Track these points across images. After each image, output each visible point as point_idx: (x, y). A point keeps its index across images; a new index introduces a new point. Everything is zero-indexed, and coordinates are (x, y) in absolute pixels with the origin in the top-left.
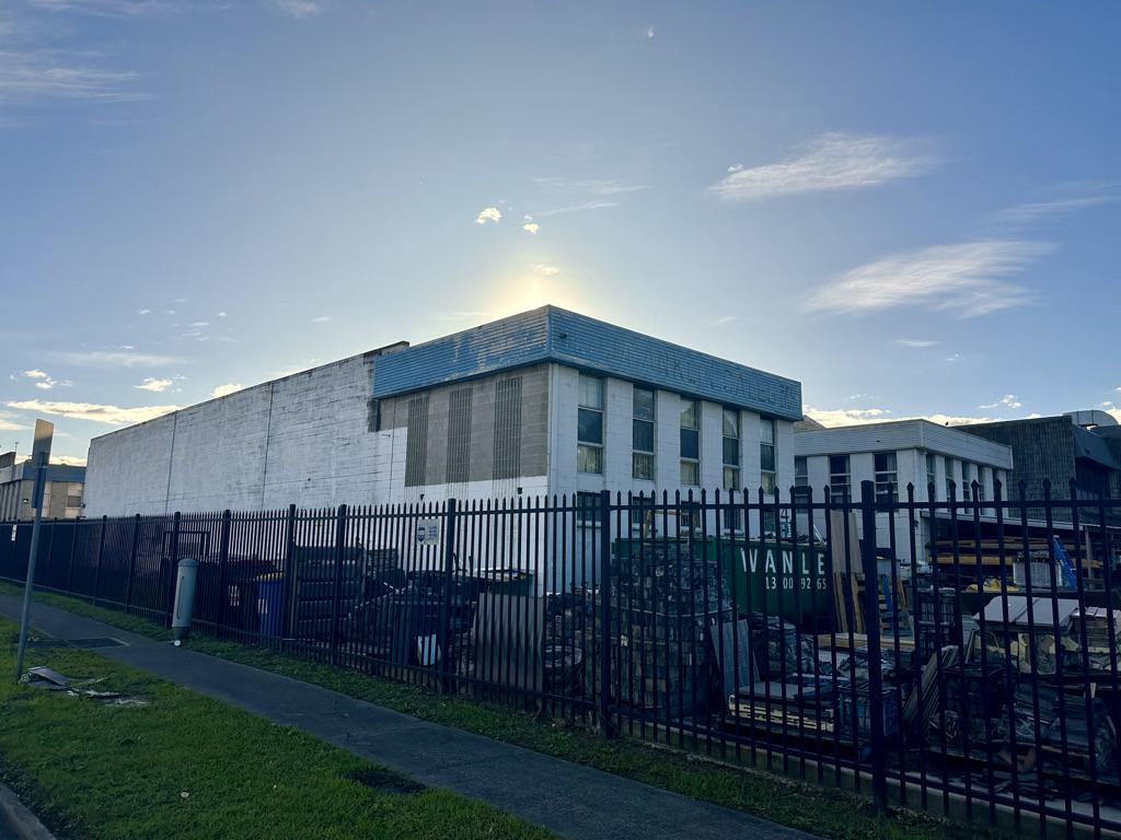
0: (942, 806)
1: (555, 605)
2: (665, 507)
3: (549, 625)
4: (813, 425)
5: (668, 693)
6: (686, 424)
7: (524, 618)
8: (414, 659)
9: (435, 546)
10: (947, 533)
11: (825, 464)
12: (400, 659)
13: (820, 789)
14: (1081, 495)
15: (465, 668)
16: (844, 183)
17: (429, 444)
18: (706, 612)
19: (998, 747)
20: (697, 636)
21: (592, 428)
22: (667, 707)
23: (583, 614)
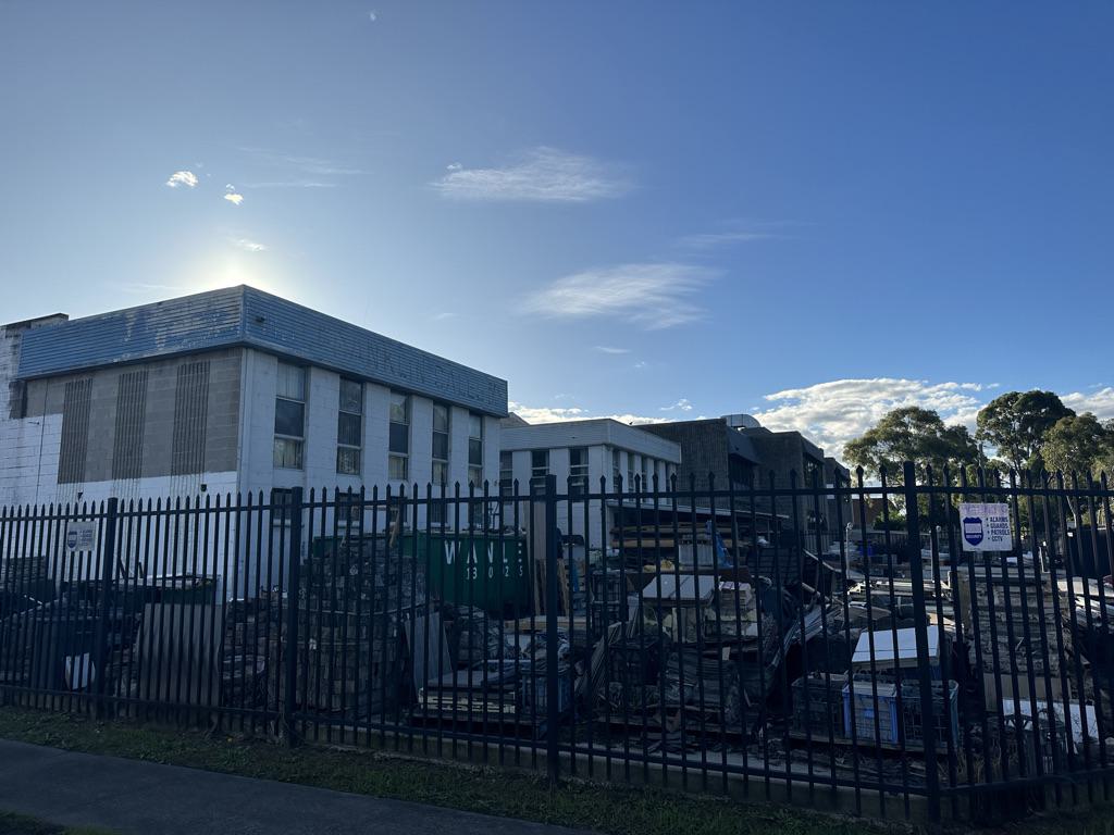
0: (605, 770)
1: (238, 612)
2: (375, 503)
3: (230, 634)
4: (518, 422)
5: (357, 694)
6: (395, 419)
7: (200, 627)
8: (60, 681)
9: (90, 553)
10: (628, 519)
11: (566, 454)
12: (42, 683)
13: (501, 770)
14: (737, 487)
15: (125, 687)
16: (555, 197)
17: (91, 434)
18: (399, 608)
19: (652, 712)
20: (390, 633)
21: (291, 421)
22: (356, 707)
23: (268, 619)
